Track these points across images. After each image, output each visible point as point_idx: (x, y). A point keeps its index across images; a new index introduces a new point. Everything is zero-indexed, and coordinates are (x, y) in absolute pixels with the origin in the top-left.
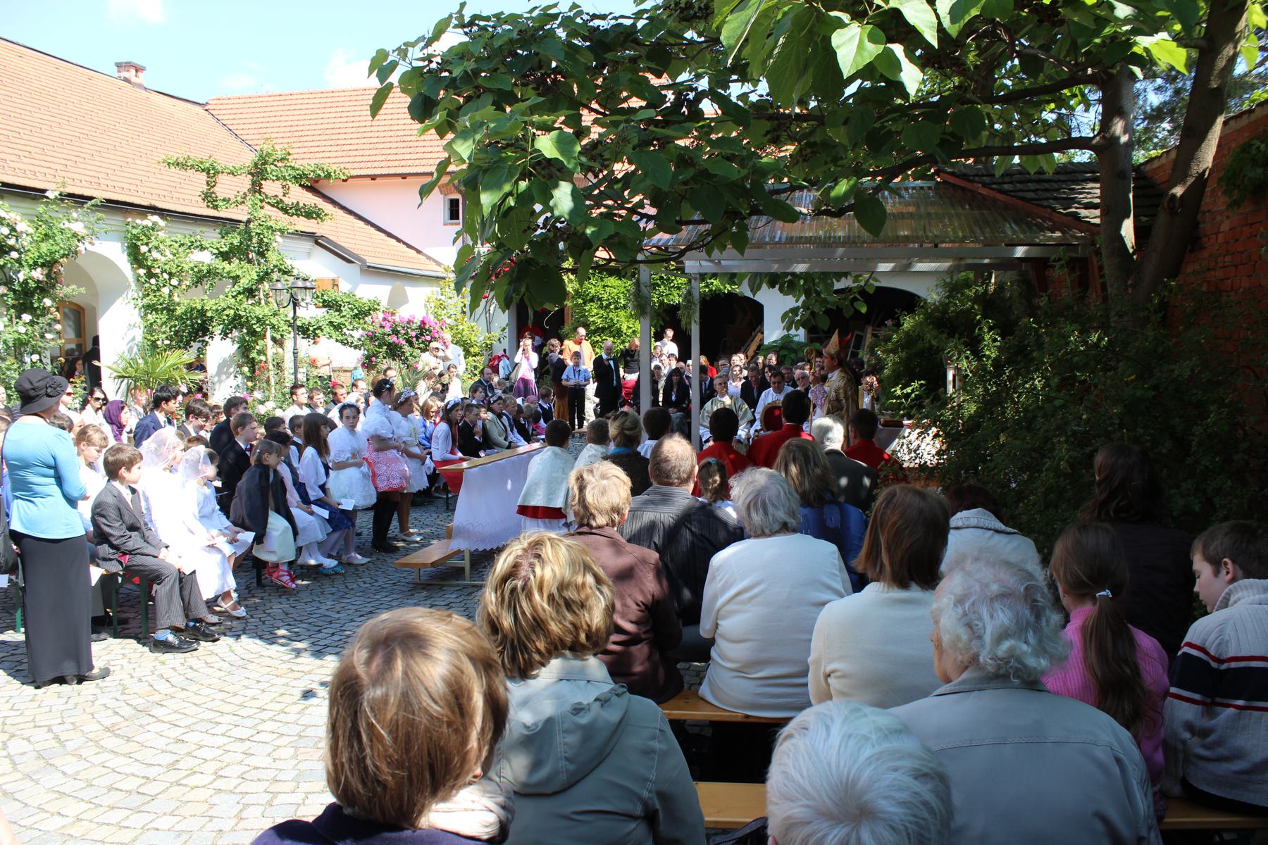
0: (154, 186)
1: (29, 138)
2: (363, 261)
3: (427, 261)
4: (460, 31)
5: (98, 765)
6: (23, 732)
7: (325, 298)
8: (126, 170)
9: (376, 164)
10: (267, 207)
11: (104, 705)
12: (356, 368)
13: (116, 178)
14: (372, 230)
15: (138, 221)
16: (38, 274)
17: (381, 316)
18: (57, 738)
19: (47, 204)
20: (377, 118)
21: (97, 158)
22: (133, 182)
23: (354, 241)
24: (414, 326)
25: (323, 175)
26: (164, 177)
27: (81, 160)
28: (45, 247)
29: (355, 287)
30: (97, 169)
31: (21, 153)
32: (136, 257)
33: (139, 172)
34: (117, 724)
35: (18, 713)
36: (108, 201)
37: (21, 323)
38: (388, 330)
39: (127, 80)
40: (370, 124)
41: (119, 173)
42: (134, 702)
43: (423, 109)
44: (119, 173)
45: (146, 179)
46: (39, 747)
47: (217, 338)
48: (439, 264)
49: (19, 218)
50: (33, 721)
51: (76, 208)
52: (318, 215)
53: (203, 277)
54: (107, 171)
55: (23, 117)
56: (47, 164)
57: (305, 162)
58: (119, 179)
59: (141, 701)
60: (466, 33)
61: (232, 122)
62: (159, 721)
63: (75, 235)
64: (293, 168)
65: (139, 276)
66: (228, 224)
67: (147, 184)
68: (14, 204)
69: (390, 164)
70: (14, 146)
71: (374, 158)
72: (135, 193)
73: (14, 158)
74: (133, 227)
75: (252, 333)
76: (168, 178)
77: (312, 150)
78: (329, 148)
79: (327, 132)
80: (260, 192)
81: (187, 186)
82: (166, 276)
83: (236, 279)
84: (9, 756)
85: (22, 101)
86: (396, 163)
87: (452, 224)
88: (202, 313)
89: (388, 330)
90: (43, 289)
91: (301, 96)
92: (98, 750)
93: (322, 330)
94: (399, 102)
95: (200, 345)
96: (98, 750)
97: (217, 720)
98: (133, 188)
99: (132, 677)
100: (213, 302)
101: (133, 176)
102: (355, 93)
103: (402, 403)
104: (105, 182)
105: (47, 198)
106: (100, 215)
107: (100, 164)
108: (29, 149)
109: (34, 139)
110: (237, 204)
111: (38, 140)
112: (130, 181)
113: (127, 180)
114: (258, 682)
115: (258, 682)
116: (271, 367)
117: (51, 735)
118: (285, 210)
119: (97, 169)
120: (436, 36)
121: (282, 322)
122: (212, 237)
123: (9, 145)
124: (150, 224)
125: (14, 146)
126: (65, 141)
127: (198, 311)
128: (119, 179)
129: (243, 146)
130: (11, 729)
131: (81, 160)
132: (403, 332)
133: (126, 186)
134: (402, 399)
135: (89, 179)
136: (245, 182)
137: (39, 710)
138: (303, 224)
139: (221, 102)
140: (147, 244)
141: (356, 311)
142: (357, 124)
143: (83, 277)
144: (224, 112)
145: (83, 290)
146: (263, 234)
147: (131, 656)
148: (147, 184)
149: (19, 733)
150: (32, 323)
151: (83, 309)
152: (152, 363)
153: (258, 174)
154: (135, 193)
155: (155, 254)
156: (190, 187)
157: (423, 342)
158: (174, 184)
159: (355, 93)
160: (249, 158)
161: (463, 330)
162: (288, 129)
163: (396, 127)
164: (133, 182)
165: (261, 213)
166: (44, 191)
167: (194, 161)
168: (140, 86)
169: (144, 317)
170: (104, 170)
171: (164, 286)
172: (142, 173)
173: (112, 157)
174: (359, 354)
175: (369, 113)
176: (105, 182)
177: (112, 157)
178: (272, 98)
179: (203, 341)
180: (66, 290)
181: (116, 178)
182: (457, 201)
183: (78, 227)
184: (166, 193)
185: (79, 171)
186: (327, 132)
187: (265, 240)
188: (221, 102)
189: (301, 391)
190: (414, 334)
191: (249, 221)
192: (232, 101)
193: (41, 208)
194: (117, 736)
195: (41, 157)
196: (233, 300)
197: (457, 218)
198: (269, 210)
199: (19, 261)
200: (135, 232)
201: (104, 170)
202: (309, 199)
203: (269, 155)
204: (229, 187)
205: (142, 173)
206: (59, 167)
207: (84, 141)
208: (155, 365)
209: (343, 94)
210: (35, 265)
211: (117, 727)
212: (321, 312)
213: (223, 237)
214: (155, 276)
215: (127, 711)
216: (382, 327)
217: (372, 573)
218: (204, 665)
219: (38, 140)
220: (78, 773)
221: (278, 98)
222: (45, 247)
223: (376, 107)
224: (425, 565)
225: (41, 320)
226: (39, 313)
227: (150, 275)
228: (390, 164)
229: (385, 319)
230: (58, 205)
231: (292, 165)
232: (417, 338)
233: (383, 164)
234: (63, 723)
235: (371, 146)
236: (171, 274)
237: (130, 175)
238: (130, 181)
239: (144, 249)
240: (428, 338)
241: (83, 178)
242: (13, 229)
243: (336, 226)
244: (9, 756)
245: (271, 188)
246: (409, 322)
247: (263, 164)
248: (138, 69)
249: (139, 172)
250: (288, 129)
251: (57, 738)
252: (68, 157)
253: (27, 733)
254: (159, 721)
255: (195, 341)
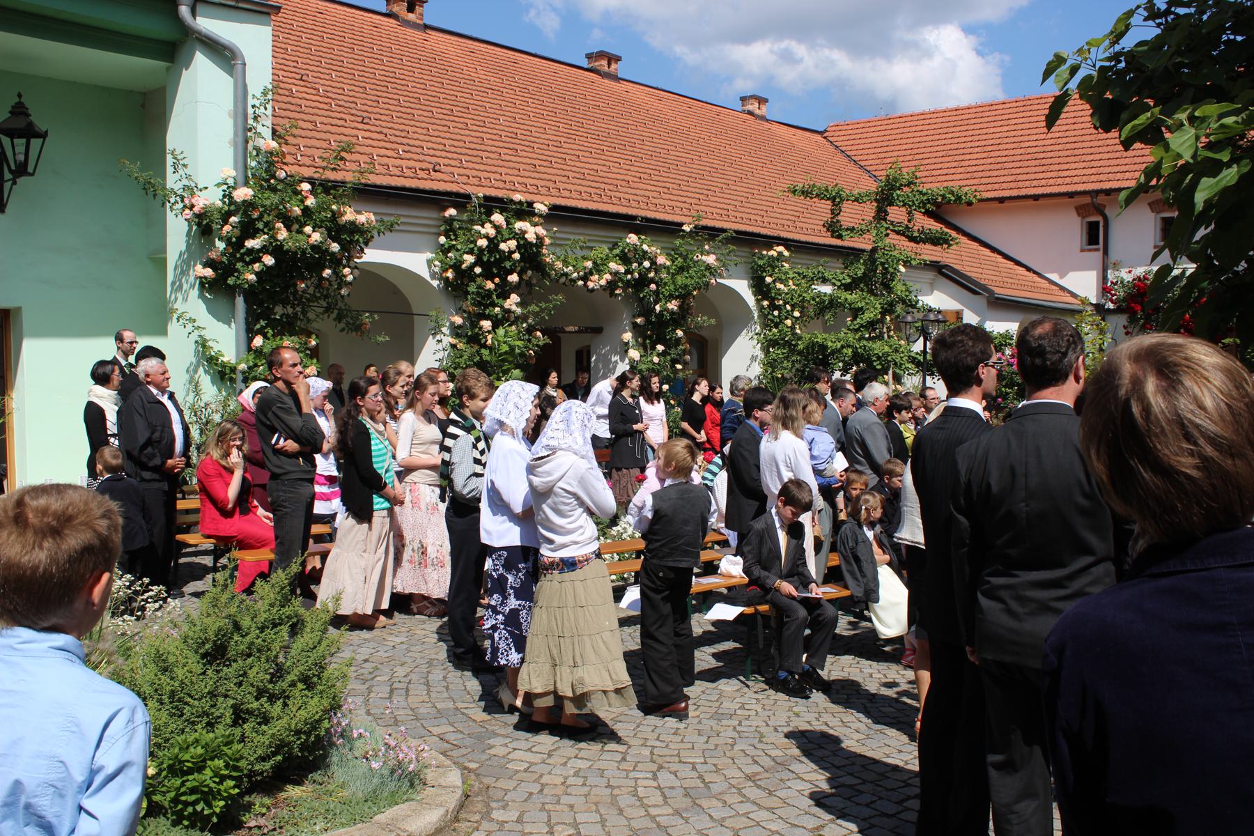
0: (778, 216)
1: (667, 175)
2: (991, 293)
3: (1061, 293)
4: (1151, 23)
5: (743, 815)
6: (670, 765)
8: (752, 201)
9: (1004, 186)
10: (892, 235)
11: (743, 751)
13: (743, 209)
14: (1000, 259)
15: (765, 252)
16: (673, 305)
18: (701, 777)
19: (683, 237)
20: (1053, 129)
21: (726, 191)
22: (760, 212)
23: (980, 270)
25: (953, 198)
26: (788, 207)
27: (712, 193)
28: (680, 280)
29: (983, 321)
30: (726, 201)
31: (661, 190)
32: (761, 289)
33: (764, 203)
34: (757, 774)
35: (663, 745)
36: (737, 232)
37: (655, 353)
39: (750, 113)
40: (1043, 136)
41: (746, 205)
42: (774, 753)
43: (1107, 117)
44: (746, 205)
45: (771, 209)
46: (687, 784)
48: (1074, 295)
49: (659, 251)
50: (678, 755)
51: (708, 240)
52: (946, 241)
53: (827, 306)
54: (735, 203)
55: (662, 155)
56: (684, 199)
57: (934, 186)
58: (746, 210)
59: (781, 753)
60: (1159, 25)
61: (850, 148)
62: (800, 778)
63: (708, 267)
64: (921, 193)
65: (762, 307)
66: (850, 255)
67: (772, 215)
68: (654, 238)
69: (1020, 184)
70: (656, 183)
71: (1002, 179)
72: (761, 224)
73: (655, 194)
74: (759, 258)
76: (791, 208)
77: (934, 173)
78: (953, 171)
79: (951, 153)
80: (885, 220)
81: (810, 216)
82: (788, 307)
83: (856, 312)
84: (659, 788)
85: (661, 142)
86: (1027, 184)
87: (1090, 250)
88: (823, 347)
90: (678, 319)
91: (923, 117)
92: (741, 799)
94: (1079, 112)
96: (741, 799)
97: (859, 787)
98: (759, 218)
99: (768, 725)
101: (758, 207)
102: (981, 109)
104: (733, 214)
105: (684, 231)
106: (732, 247)
107: (729, 196)
108: (667, 185)
109: (671, 176)
110: (862, 232)
111: (674, 176)
112: (756, 212)
113: (753, 212)
114: (900, 751)
115: (900, 751)
117: (695, 774)
118: (912, 239)
119: (726, 201)
120: (1117, 36)
122: (835, 269)
123: (652, 183)
124: (775, 254)
125: (656, 183)
126: (697, 176)
127: (820, 345)
128: (746, 210)
129: (861, 172)
130: (659, 760)
131: (712, 193)
133: (753, 217)
135: (719, 211)
136: (869, 210)
137: (682, 746)
138: (930, 253)
139: (840, 128)
140: (771, 276)
142: (983, 143)
143: (712, 311)
144: (841, 138)
145: (713, 321)
146: (888, 263)
147: (765, 702)
148: (772, 215)
149: (666, 765)
150: (663, 354)
151: (706, 341)
153: (884, 199)
154: (761, 224)
155: (780, 286)
156: (813, 216)
158: (798, 214)
159: (981, 109)
160: (872, 186)
162: (908, 152)
163: (1027, 144)
164: (760, 212)
165: (887, 241)
166: (682, 224)
167: (820, 189)
168: (763, 118)
169: (767, 352)
170: (733, 203)
171: (787, 318)
172: (767, 203)
173: (738, 189)
175: (1044, 124)
176: (733, 214)
177: (738, 189)
178: (892, 121)
180: (701, 320)
181: (743, 209)
182: (1097, 223)
183: (711, 259)
184: (789, 223)
185: (711, 204)
186: (951, 153)
187: (891, 270)
188: (840, 128)
191: (874, 250)
192: (850, 127)
193: (678, 242)
194: (759, 787)
195: (677, 192)
197: (1097, 243)
198: (894, 239)
199: (657, 293)
200: (761, 263)
201: (733, 203)
202: (932, 225)
203: (895, 179)
204: (851, 215)
205: (767, 203)
206: (693, 201)
207: (714, 175)
209: (967, 111)
210: (671, 297)
211: (757, 777)
213: (846, 268)
214: (778, 308)
215: (767, 762)
218: (840, 724)
219: (674, 176)
220: (724, 819)
221: (910, 119)
222: (680, 280)
223: (1052, 119)
225: (673, 351)
226: (671, 344)
227: (773, 306)
228: (1020, 184)
230: (693, 238)
231: (920, 189)
233: (1012, 185)
234: (706, 763)
235: (999, 166)
236: (793, 306)
237: (755, 206)
238: (756, 212)
239: (768, 280)
241: (714, 210)
242: (653, 263)
243: (961, 255)
244: (659, 788)
245: (896, 214)
247: (889, 190)
248: (762, 101)
249: (764, 203)
250: (908, 152)
251: (701, 777)
252: (701, 191)
253: (674, 767)
254: (800, 778)
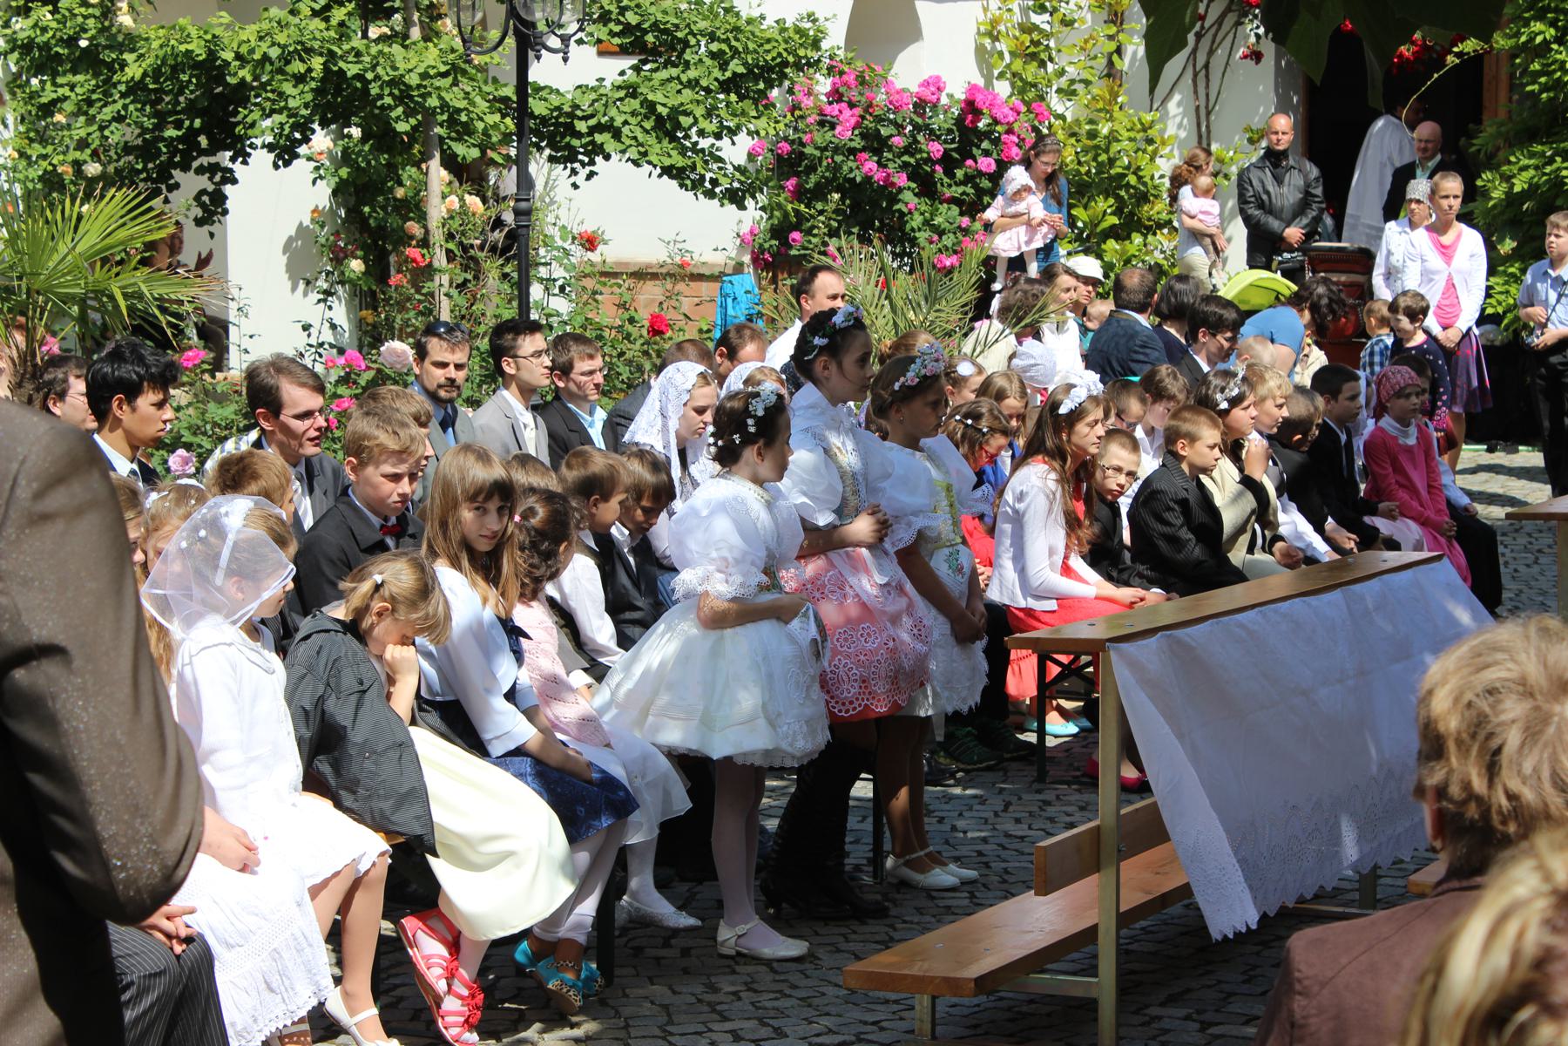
7: (632, 18)
12: (739, 268)
17: (824, 85)
24: (940, 121)
38: (845, 133)
47: (261, 159)
75: (381, 135)
89: (845, 133)
93: (617, 135)
95: (204, 182)
100: (249, 32)
103: (909, 393)
116: (440, 260)
121: (483, 105)
127: (197, 65)
132: (899, 142)
134: (911, 377)
141: (736, 67)
152: (34, 238)
157: (969, 179)
161: (1113, 137)
174: (752, 216)
179: (213, 169)
189: (530, 344)
190: (936, 149)
196: (317, 23)
208: (38, 249)
212: (614, 69)
216: (826, 123)
217: (765, 1000)
224: (953, 985)
229: (836, 95)
232: (949, 163)
240: (987, 164)
246: (920, 105)
255: (185, 168)
